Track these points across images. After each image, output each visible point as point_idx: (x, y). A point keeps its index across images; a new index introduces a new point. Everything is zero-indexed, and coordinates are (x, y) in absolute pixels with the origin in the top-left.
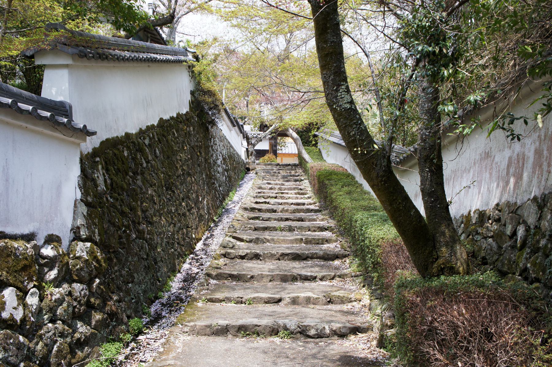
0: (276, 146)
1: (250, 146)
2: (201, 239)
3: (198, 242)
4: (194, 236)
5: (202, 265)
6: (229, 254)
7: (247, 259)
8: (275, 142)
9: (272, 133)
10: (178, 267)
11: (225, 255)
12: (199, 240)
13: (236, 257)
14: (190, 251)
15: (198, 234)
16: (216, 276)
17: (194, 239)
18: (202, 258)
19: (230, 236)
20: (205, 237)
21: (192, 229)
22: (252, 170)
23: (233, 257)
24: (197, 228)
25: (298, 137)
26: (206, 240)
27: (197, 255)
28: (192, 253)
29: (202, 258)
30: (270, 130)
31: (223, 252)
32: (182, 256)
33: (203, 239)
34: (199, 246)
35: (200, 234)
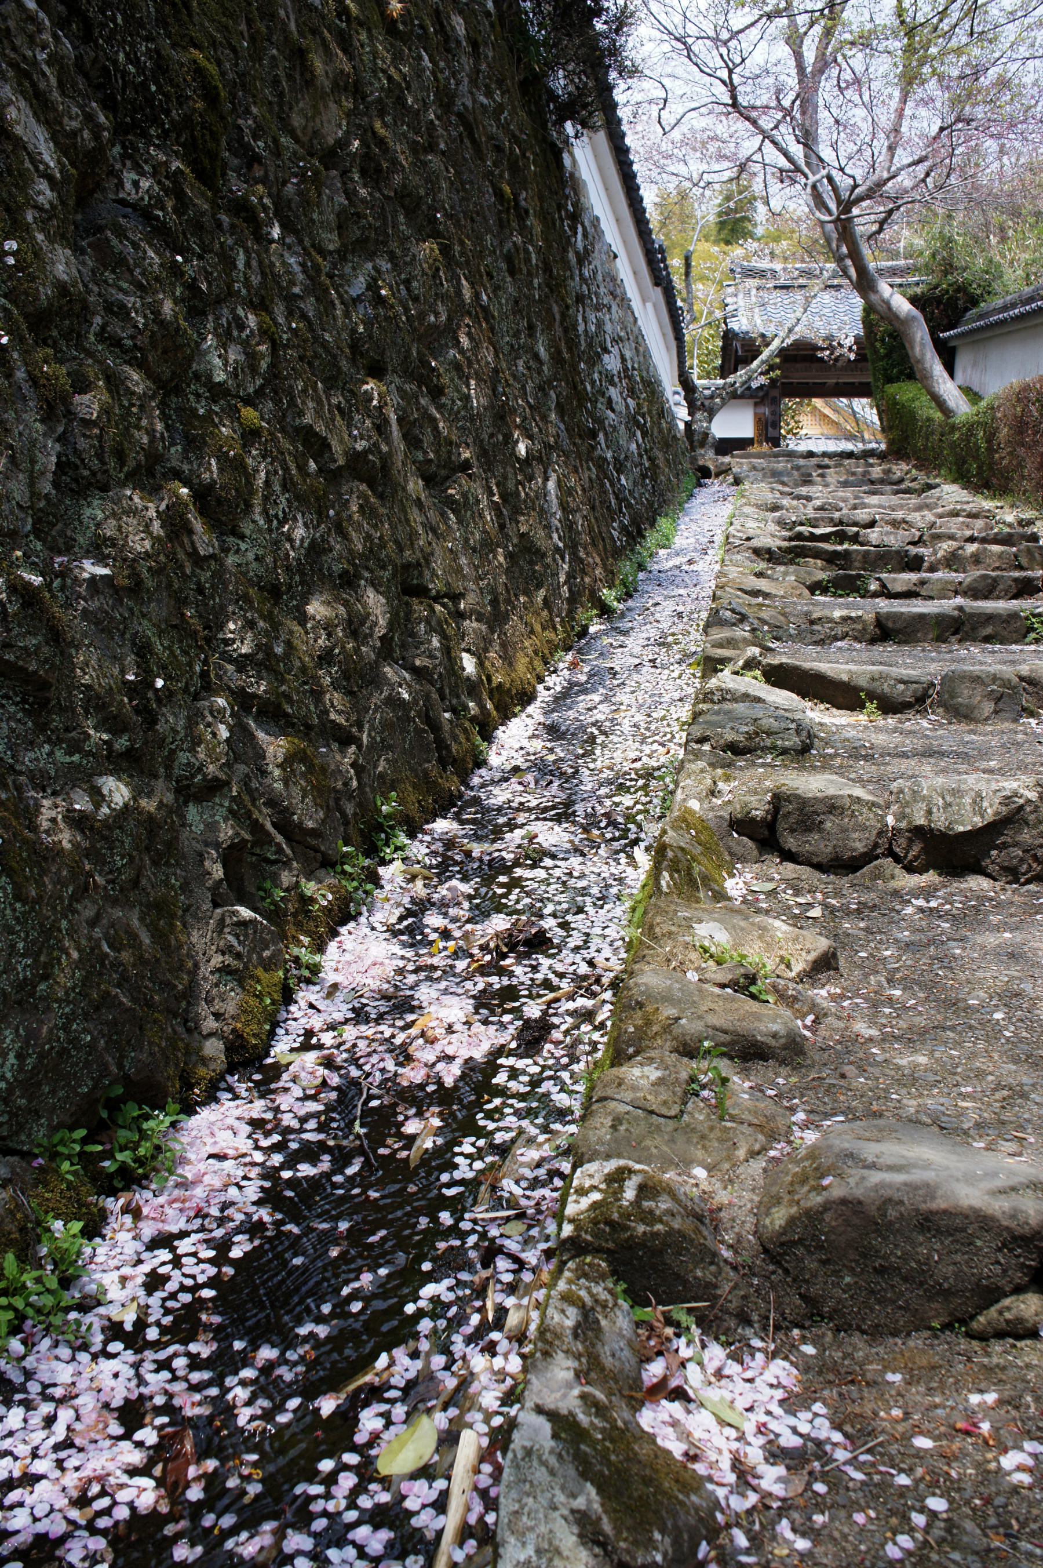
0: (776, 425)
1: (698, 415)
2: (527, 698)
3: (506, 715)
4: (469, 664)
5: (540, 943)
6: (809, 814)
7: (1012, 874)
8: (773, 413)
9: (772, 368)
10: (219, 1010)
11: (767, 833)
12: (513, 700)
13: (886, 847)
14: (426, 784)
15: (508, 660)
16: (776, 1251)
17: (473, 688)
18: (535, 856)
19: (750, 665)
20: (556, 682)
21: (461, 616)
22: (717, 475)
23: (859, 844)
24: (496, 619)
25: (916, 312)
26: (563, 698)
27: (490, 825)
28: (445, 804)
29: (535, 856)
30: (764, 356)
31: (749, 788)
32: (298, 865)
33: (543, 695)
34: (516, 739)
35: (522, 663)
